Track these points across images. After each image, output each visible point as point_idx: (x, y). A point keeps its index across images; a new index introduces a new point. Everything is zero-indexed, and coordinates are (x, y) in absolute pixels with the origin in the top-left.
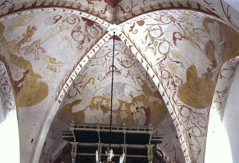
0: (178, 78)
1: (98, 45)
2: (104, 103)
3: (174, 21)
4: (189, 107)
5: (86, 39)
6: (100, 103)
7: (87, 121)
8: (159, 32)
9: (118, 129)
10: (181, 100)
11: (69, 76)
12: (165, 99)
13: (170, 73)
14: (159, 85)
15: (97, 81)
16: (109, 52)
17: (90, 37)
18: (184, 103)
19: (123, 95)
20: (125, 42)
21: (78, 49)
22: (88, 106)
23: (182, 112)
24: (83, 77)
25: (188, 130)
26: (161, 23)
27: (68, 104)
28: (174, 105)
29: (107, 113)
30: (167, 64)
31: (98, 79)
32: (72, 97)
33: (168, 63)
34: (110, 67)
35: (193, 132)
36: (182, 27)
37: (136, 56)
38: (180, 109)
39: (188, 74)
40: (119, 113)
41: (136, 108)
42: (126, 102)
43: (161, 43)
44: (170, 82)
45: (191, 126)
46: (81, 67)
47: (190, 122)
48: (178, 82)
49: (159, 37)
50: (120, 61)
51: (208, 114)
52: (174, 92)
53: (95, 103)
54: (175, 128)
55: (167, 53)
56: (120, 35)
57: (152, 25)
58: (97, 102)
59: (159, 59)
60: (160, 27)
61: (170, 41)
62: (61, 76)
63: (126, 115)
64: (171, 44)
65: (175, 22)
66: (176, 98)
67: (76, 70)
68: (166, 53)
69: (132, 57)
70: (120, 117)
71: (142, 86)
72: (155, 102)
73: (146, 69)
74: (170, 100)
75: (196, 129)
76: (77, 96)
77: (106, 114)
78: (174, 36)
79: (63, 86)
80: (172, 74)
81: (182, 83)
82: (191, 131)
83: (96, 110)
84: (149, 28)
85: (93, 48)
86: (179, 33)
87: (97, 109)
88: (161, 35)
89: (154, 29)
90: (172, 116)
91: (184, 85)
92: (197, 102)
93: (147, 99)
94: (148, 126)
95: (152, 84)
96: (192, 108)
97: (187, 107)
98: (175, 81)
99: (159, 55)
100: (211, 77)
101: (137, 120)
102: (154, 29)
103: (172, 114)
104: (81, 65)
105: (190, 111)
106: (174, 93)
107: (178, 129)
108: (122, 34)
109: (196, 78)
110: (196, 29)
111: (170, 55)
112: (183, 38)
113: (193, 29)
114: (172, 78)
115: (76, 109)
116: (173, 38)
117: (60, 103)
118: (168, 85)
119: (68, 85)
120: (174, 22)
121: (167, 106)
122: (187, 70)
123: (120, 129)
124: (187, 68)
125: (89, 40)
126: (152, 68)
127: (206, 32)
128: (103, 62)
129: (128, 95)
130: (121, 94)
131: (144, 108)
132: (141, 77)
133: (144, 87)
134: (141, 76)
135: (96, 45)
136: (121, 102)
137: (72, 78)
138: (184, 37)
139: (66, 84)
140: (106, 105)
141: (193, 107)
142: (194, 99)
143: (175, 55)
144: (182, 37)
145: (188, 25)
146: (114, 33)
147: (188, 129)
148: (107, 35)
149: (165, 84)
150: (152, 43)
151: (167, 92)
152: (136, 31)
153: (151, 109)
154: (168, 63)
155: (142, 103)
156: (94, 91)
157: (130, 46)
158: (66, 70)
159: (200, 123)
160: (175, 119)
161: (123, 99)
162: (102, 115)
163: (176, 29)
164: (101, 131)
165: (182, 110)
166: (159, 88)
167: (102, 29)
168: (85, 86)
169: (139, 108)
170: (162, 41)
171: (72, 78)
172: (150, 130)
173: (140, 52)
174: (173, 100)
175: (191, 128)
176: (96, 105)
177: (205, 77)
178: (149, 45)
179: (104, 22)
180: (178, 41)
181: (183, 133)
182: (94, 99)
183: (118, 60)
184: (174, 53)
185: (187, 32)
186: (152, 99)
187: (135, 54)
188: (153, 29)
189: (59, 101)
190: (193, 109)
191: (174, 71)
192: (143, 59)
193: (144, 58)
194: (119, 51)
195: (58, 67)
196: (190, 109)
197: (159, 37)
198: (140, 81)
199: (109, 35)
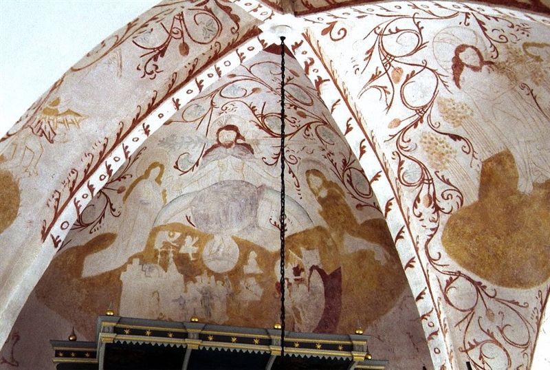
1: (217, 70)
2: (189, 247)
4: (476, 278)
5: (175, 45)
6: (174, 247)
7: (129, 308)
8: (410, 41)
9: (256, 341)
10: (454, 255)
11: (100, 161)
12: (405, 249)
13: (425, 169)
14: (389, 204)
15: (171, 175)
16: (231, 83)
17: (187, 40)
18: (458, 262)
19: (254, 225)
20: (307, 66)
21: (142, 73)
22: (135, 256)
23: (452, 293)
24: (132, 160)
25: (466, 351)
27: (74, 248)
28: (428, 271)
29: (195, 281)
30: (421, 142)
31: (176, 167)
32: (88, 225)
33: (426, 138)
34: (220, 130)
35: (481, 358)
36: (489, 32)
37: (332, 110)
38: (444, 284)
39: (485, 178)
40: (236, 283)
41: (294, 269)
42: (261, 249)
43: (413, 74)
44: (421, 197)
45: (478, 340)
46: (147, 132)
47: (474, 326)
48: (448, 199)
49: (408, 55)
50: (259, 111)
51: (540, 307)
52: (432, 229)
53: (158, 246)
54: (424, 341)
55: (426, 106)
56: (297, 45)
57: (394, 18)
58: (166, 244)
59: (398, 122)
60: (417, 25)
61: (440, 71)
62: (70, 156)
63: (260, 291)
64: (444, 79)
65: (471, 16)
66: (436, 247)
67: (128, 141)
68: (423, 107)
69: (302, 105)
70: (238, 298)
71: (322, 201)
72: (363, 255)
74: (417, 254)
75: (490, 350)
76: (103, 222)
77: (190, 285)
79: (72, 194)
80: (432, 172)
82: (474, 355)
83: (161, 269)
84: (382, 27)
85: (199, 77)
86: (476, 49)
87: (165, 266)
88: (417, 49)
89: (398, 31)
90: (419, 304)
91: (468, 208)
92: (504, 265)
93: (333, 242)
94: (353, 336)
95: (360, 198)
96: (484, 282)
97: (469, 279)
98: (438, 196)
99: (399, 112)
101: (294, 308)
102: (398, 31)
103: (419, 297)
104: (148, 126)
105: (478, 290)
106: (433, 232)
107: (436, 346)
108: (302, 41)
110: (534, 45)
112: (485, 67)
113: (526, 45)
114: (429, 184)
115: (96, 265)
117: (56, 245)
118: (415, 206)
119: (91, 188)
121: (409, 273)
122: (485, 163)
123: (262, 342)
124: (486, 158)
125: (185, 49)
126: (375, 151)
128: (201, 115)
129: (269, 227)
130: (246, 222)
131: (321, 272)
133: (331, 204)
134: (324, 167)
135: (211, 69)
136: (245, 248)
137: (108, 167)
138: (490, 63)
139: (85, 186)
140: (194, 255)
141: (488, 280)
142: (495, 255)
144: (482, 62)
145: (512, 31)
146: (283, 38)
147: (468, 347)
148: (253, 42)
149: (407, 202)
150: (383, 71)
151: (411, 226)
152: (342, 33)
153: (345, 277)
154: (426, 138)
155: (317, 254)
156: (160, 207)
157: (320, 81)
158: (87, 137)
159: (507, 332)
160: (428, 315)
161: (254, 238)
162: (180, 288)
164: (201, 348)
165: (452, 285)
166: (389, 213)
167: (236, 19)
168: (132, 187)
169: (303, 270)
170: (417, 69)
171: (108, 167)
172: (357, 348)
173: (346, 100)
174: (427, 253)
175: (477, 344)
176: (161, 253)
177: (542, 193)
178: (374, 78)
179: (260, 6)
180: (466, 74)
181: (450, 360)
182: (154, 232)
183: (253, 109)
184: (449, 107)
185: (501, 48)
186: (352, 244)
188: (394, 31)
189: (54, 241)
190: (490, 287)
192: (353, 123)
193: (356, 120)
194: (262, 82)
195: (61, 126)
196: (477, 285)
197: (408, 55)
198: (316, 181)
199: (262, 42)
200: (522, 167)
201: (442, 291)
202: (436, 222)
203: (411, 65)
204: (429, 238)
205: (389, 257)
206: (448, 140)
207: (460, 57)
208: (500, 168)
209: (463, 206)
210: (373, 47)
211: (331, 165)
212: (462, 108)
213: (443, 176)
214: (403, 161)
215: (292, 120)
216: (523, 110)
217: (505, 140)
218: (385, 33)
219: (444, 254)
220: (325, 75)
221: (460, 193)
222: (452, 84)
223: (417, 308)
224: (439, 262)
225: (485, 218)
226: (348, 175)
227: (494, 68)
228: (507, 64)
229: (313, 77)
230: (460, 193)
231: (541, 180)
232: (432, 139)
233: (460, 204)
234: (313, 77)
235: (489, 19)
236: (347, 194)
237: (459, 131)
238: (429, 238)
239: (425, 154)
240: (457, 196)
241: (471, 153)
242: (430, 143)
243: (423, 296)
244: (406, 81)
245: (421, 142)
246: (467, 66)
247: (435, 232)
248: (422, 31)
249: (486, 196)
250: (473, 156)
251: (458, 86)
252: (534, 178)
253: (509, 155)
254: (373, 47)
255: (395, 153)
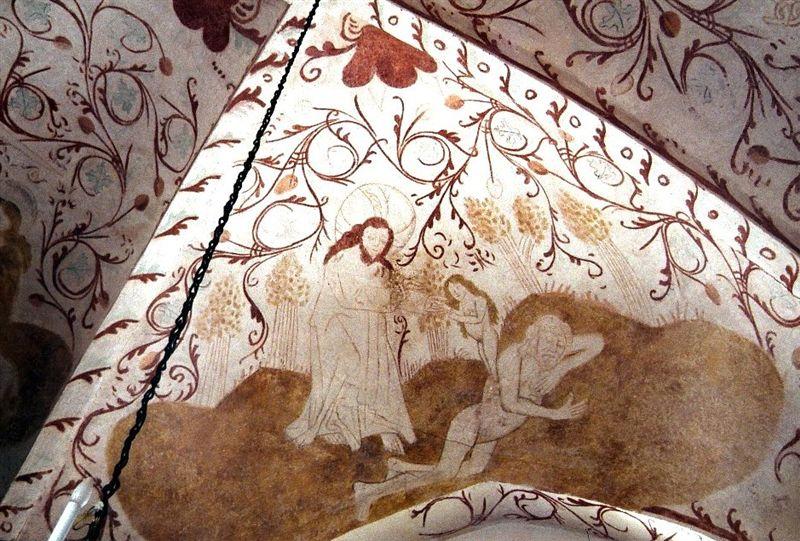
0: (190, 365)
3: (438, 190)
8: (341, 161)
26: (391, 149)
30: (217, 285)
33: (226, 285)
36: (429, 232)
39: (246, 389)
43: (300, 201)
44: (148, 350)
48: (175, 378)
49: (320, 175)
55: (270, 249)
60: (368, 154)
65: (436, 199)
69: (103, 114)
73: (167, 223)
78: (366, 225)
81: (189, 395)
84: (341, 117)
86: (391, 237)
88: (335, 179)
89: (345, 139)
91: (191, 409)
92: (175, 513)
95: (52, 289)
100: (356, 478)
102: (345, 139)
103: (27, 478)
106: (116, 405)
109: (273, 430)
111: (267, 267)
112: (378, 265)
116: (349, 229)
118: (130, 355)
120: (431, 196)
122: (263, 371)
124: (270, 366)
127: (499, 330)
132: (26, 218)
134: (35, 213)
138: (388, 265)
141: (130, 517)
143: (280, 289)
144: (381, 257)
150: (281, 166)
152: (315, 73)
154: (226, 285)
157: (252, 96)
160: (15, 510)
163: (403, 215)
166: (108, 337)
170: (310, 200)
177: (321, 455)
180: (352, 254)
183: (21, 60)
184: (288, 275)
185: (421, 260)
187: (218, 133)
188: (342, 135)
191: (209, 327)
197: (320, 175)
200: (316, 407)
201: (53, 490)
202: (133, 395)
203: (310, 189)
204: (106, 408)
205: (15, 392)
206: (246, 310)
207: (366, 230)
208: (280, 390)
209: (188, 401)
210: (307, 128)
211: (50, 220)
212: (300, 288)
213: (196, 347)
214: (178, 289)
215: (58, 120)
216: (373, 345)
217: (315, 362)
218: (332, 127)
219: (103, 443)
220: (266, 96)
221: (196, 386)
222: (324, 250)
223: (7, 489)
224: (87, 450)
225: (203, 437)
226: (64, 249)
227: (386, 274)
228: (406, 282)
229: (251, 82)
230: (196, 386)
231: (334, 440)
232: (231, 293)
233: (184, 396)
234: (251, 82)
235: (453, 218)
236: (31, 270)
237: (267, 315)
238: (106, 408)
239: (207, 302)
240: (190, 384)
241: (256, 347)
242: (224, 295)
243: (34, 479)
244: (285, 201)
245: (217, 285)
246: (361, 247)
247: (61, 420)
248: (365, 165)
249: (230, 411)
250: (256, 352)
251: (327, 259)
252: (324, 431)
253: (306, 383)
254: (307, 128)
255: (182, 270)
